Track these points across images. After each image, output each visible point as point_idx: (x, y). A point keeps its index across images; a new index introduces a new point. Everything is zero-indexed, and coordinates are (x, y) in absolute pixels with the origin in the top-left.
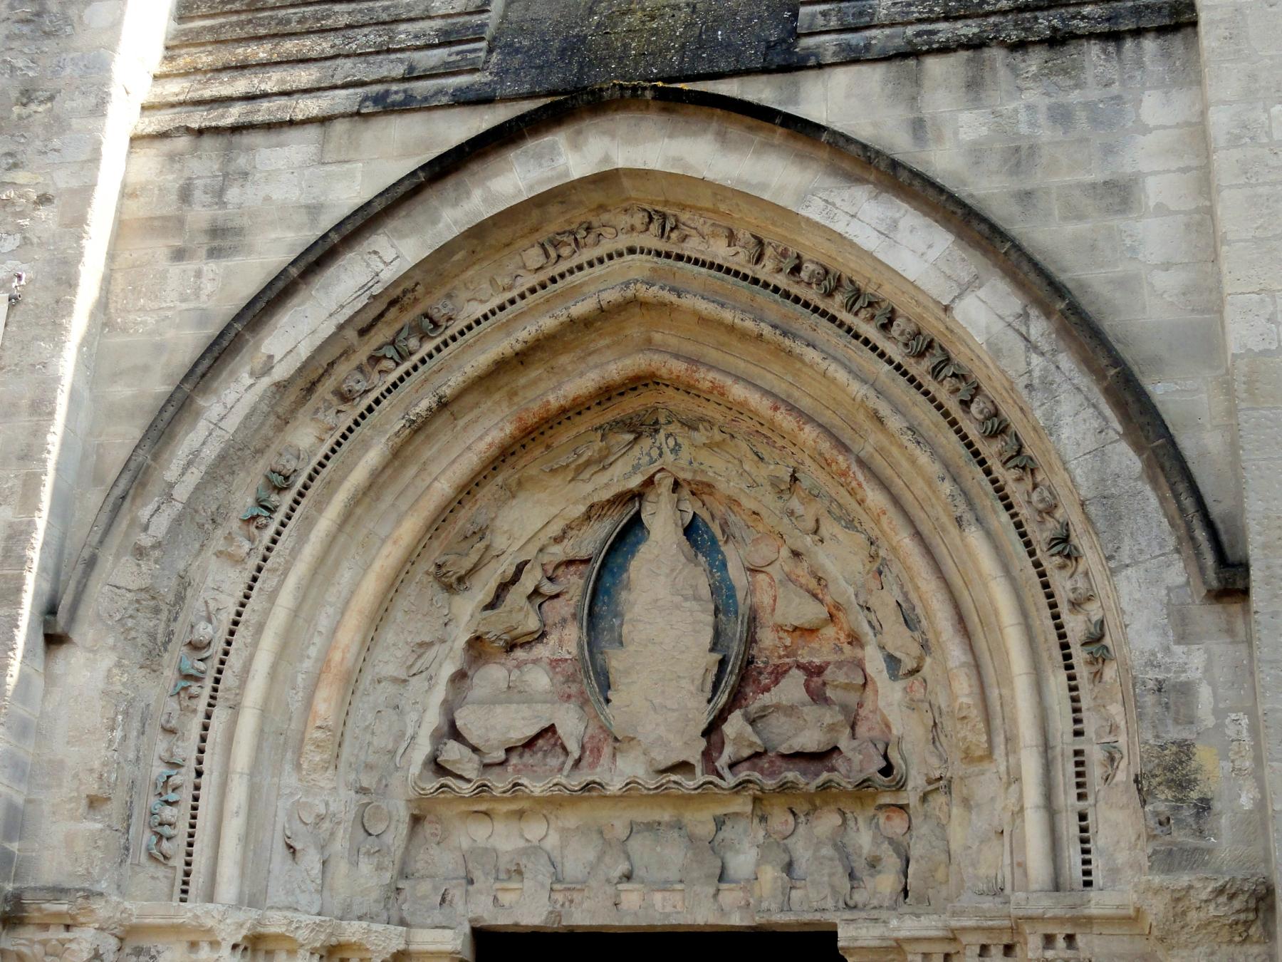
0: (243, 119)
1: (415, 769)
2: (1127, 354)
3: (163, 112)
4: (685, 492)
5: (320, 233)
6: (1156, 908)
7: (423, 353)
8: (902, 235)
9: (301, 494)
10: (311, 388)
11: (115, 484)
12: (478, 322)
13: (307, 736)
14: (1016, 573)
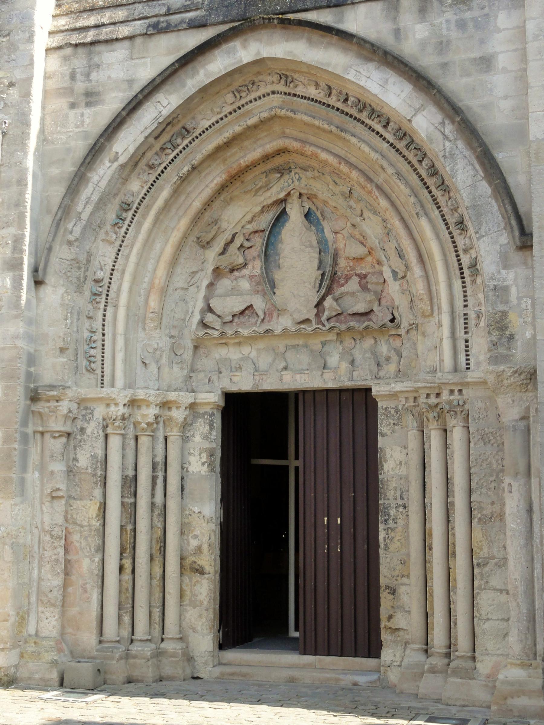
0: (95, 39)
1: (194, 326)
2: (487, 140)
3: (58, 35)
4: (305, 198)
5: (134, 93)
6: (491, 379)
7: (183, 145)
8: (390, 86)
9: (136, 212)
10: (136, 165)
11: (56, 215)
12: (207, 129)
13: (147, 316)
14: (441, 237)
